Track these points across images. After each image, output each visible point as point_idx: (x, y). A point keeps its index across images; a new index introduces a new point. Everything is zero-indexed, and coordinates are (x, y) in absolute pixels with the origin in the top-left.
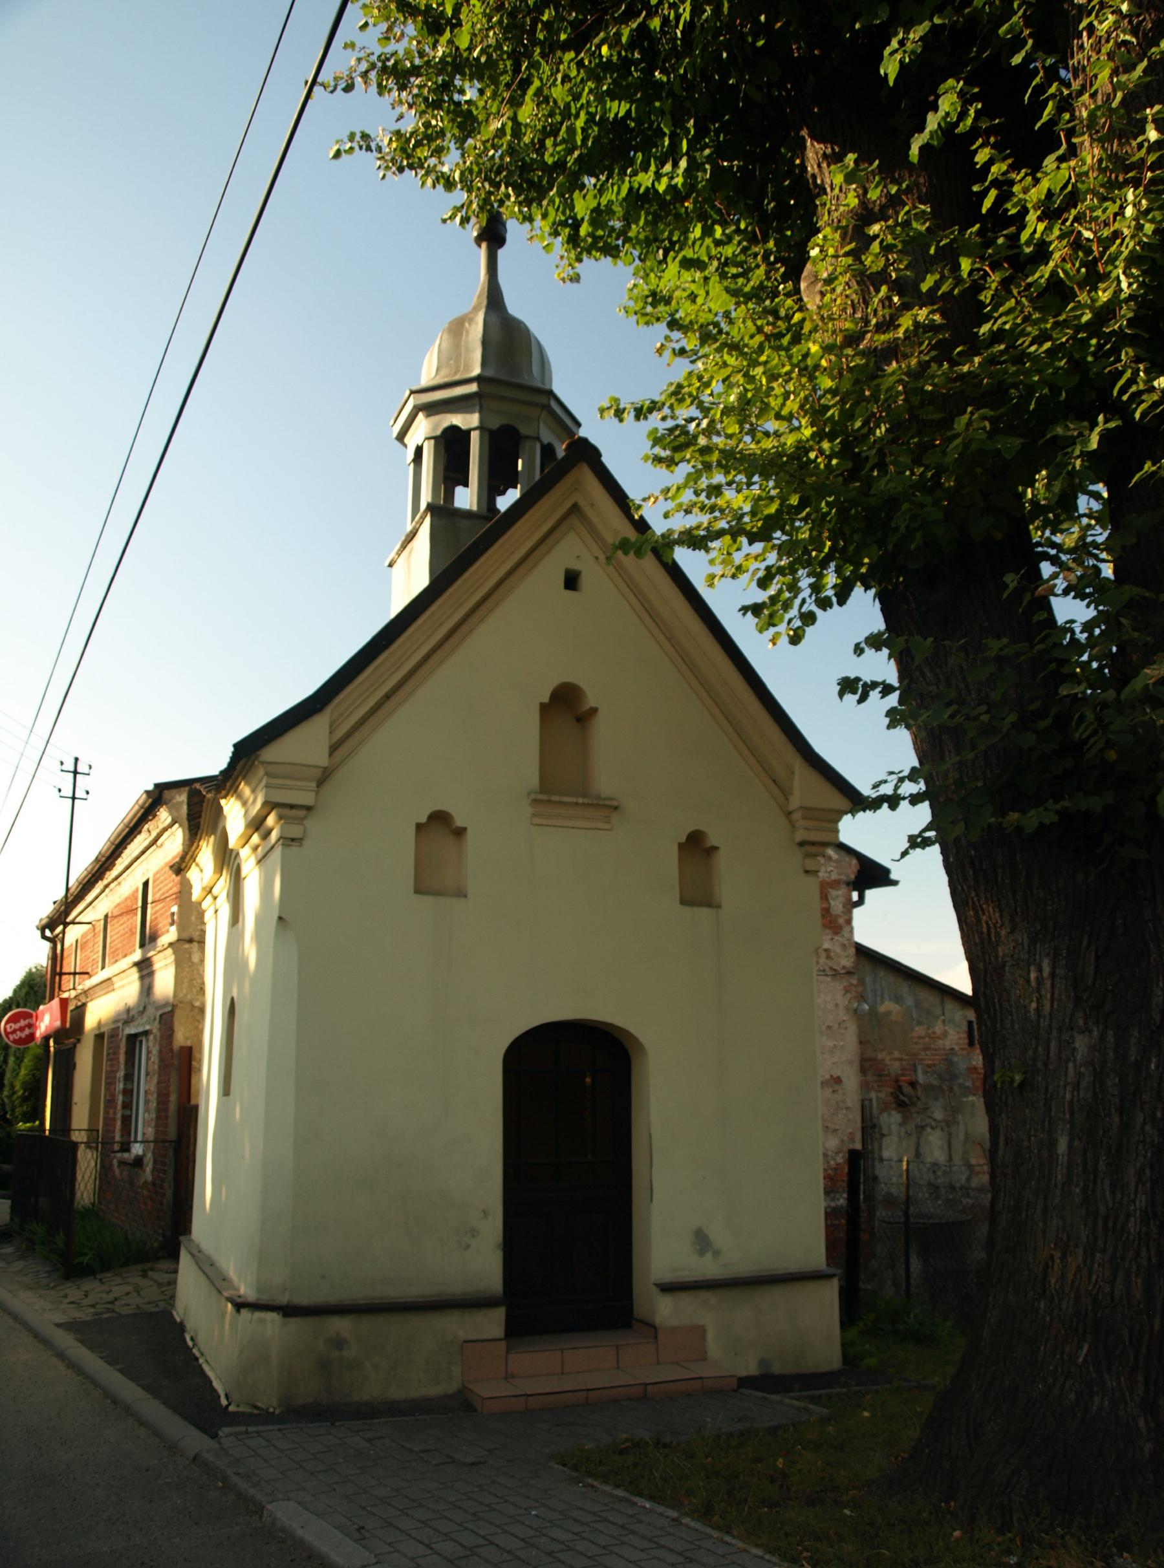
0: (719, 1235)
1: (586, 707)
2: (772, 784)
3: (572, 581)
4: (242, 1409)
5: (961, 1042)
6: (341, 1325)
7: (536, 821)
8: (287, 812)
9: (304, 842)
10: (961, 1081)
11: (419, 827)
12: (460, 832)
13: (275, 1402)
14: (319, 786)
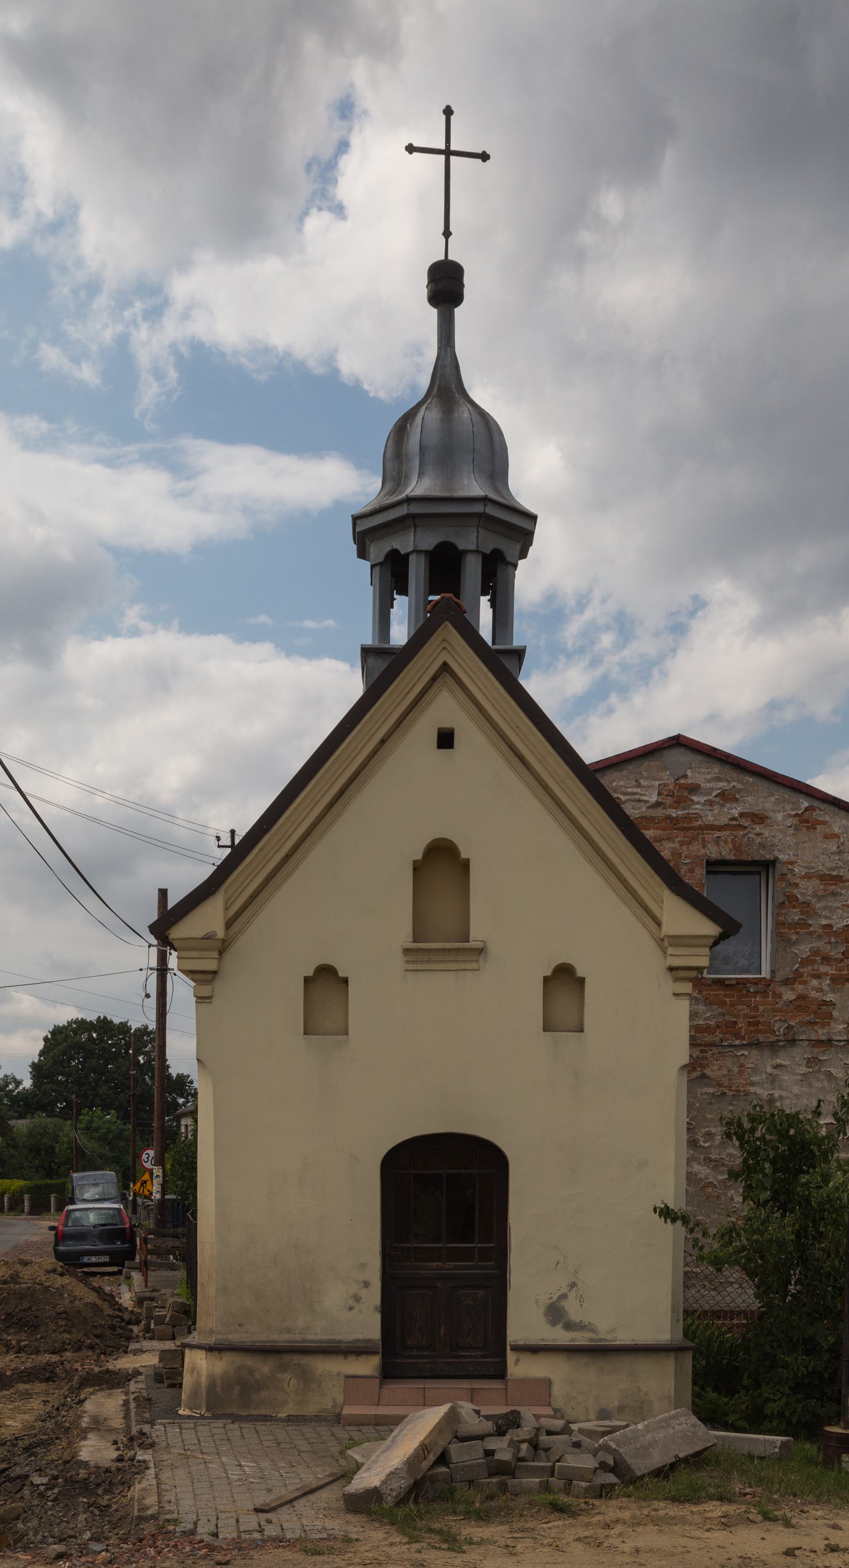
3: (446, 739)
8: (199, 976)
9: (213, 1000)
11: (307, 980)
12: (346, 981)
14: (221, 953)
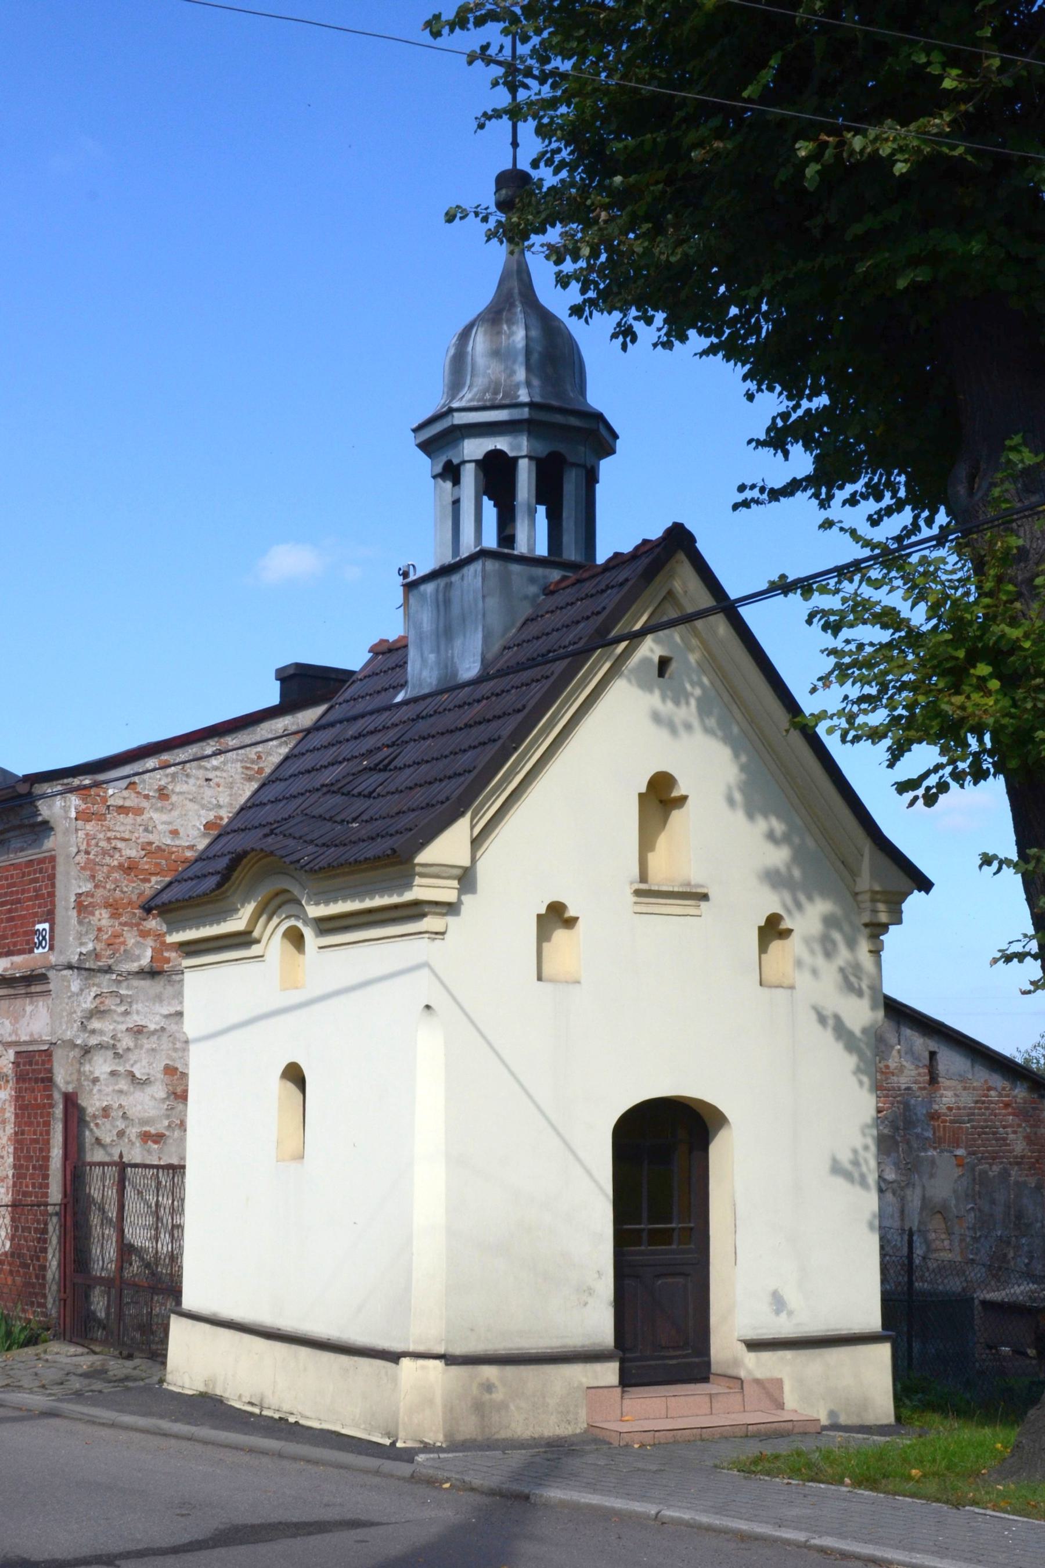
0: (792, 1297)
1: (675, 794)
2: (842, 866)
4: (410, 1444)
5: (921, 1079)
6: (490, 1372)
7: (639, 909)
10: (919, 1130)
11: (539, 917)
13: (441, 1437)
